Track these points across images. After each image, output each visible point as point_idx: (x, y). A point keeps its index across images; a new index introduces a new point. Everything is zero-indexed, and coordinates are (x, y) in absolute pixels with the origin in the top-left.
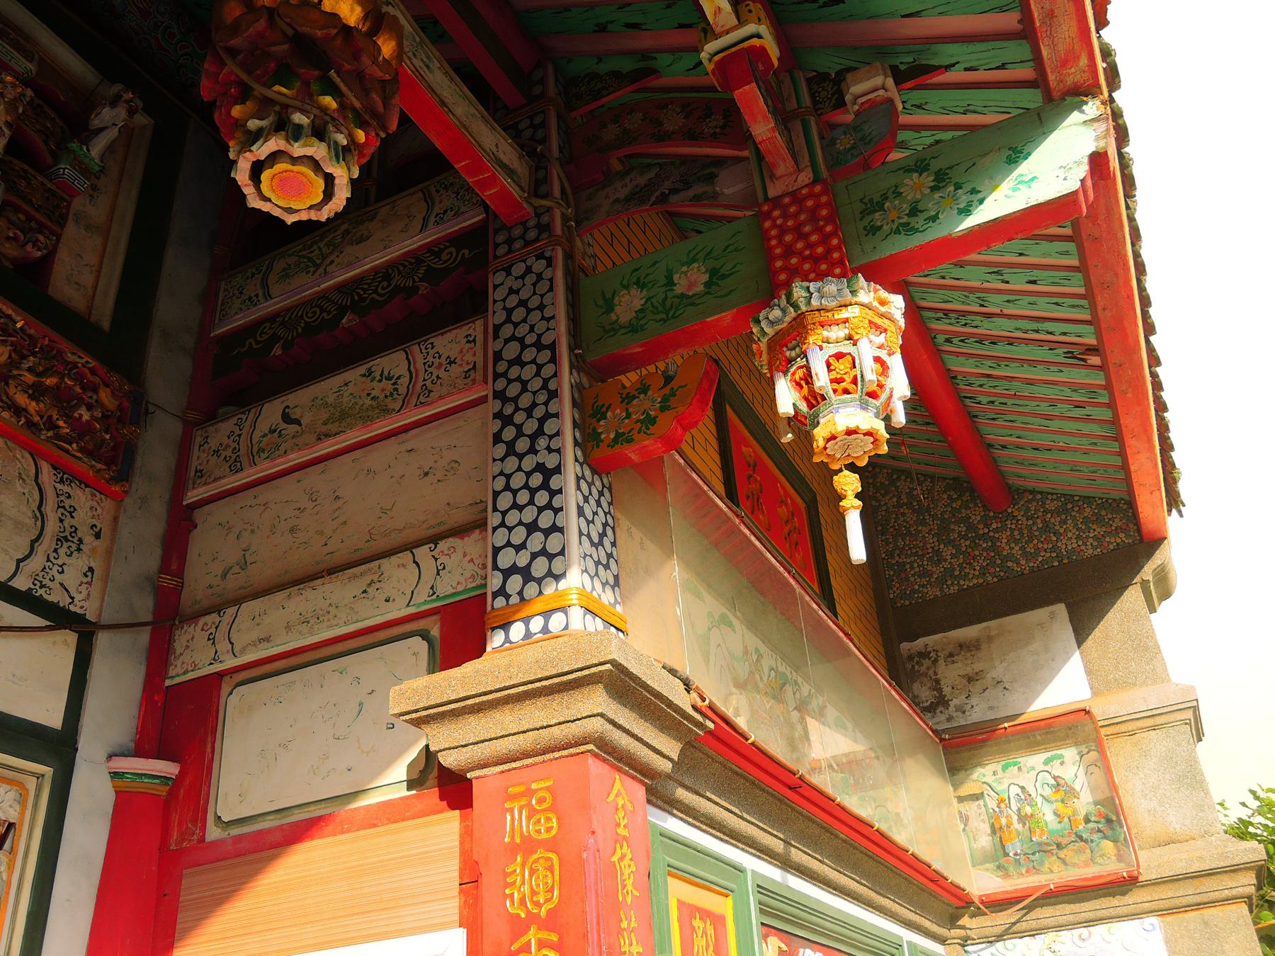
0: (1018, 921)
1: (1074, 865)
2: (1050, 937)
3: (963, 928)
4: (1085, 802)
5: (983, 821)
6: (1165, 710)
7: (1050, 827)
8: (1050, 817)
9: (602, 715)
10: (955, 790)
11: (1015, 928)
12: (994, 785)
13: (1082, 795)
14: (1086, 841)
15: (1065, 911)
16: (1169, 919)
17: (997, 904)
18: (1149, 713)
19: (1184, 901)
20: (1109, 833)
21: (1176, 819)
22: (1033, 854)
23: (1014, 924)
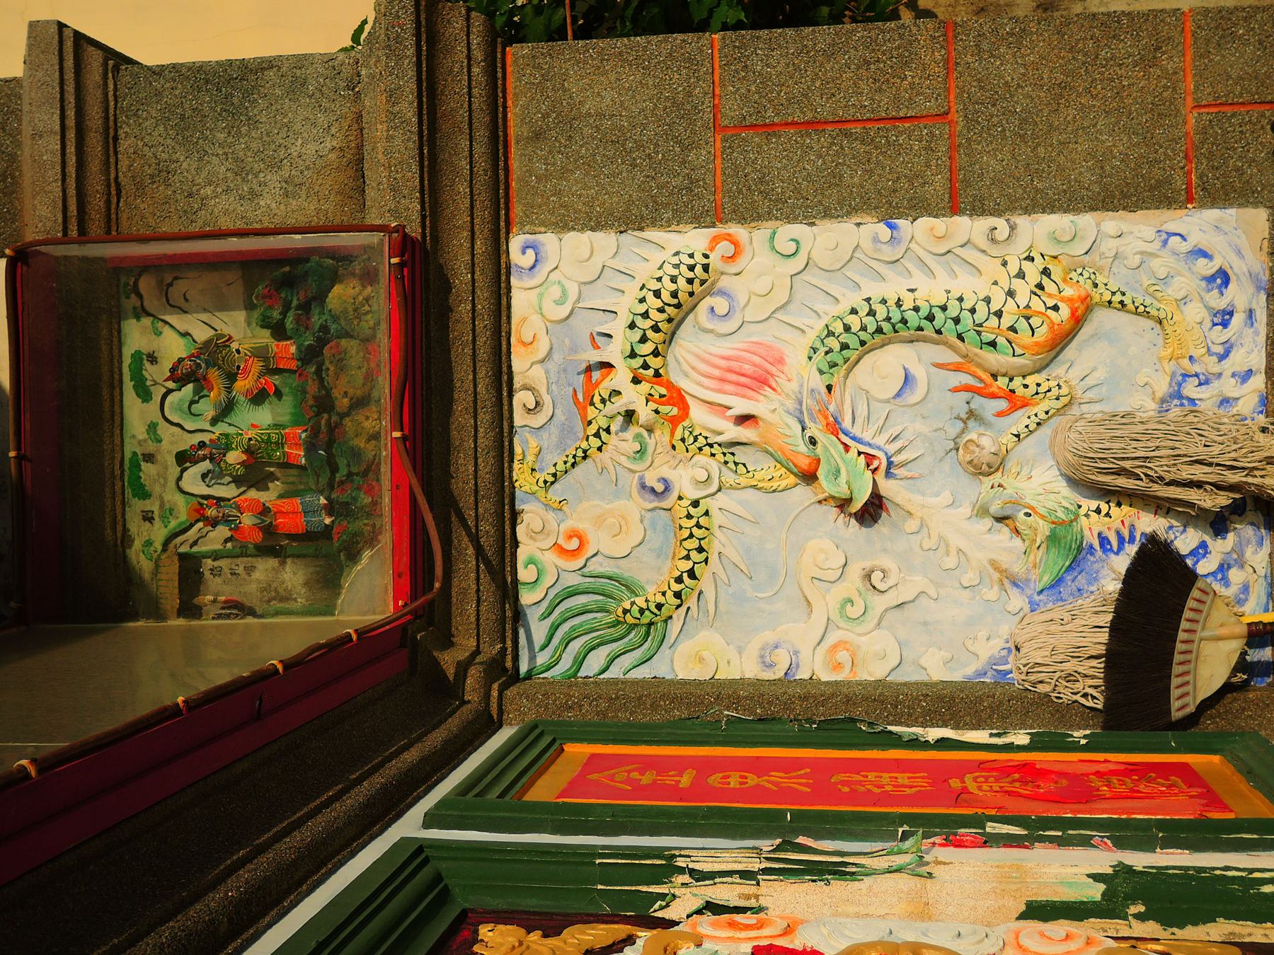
0: (475, 539)
1: (370, 377)
2: (522, 478)
3: (463, 668)
4: (239, 328)
5: (250, 569)
6: (71, 98)
7: (286, 419)
8: (263, 416)
9: (886, 610)
10: (157, 613)
11: (490, 553)
12: (173, 524)
13: (227, 330)
14: (322, 342)
15: (645, 717)
16: (517, 210)
17: (421, 572)
18: (71, 135)
19: (482, 164)
20: (313, 285)
21: (313, 141)
22: (334, 469)
23: (479, 550)
